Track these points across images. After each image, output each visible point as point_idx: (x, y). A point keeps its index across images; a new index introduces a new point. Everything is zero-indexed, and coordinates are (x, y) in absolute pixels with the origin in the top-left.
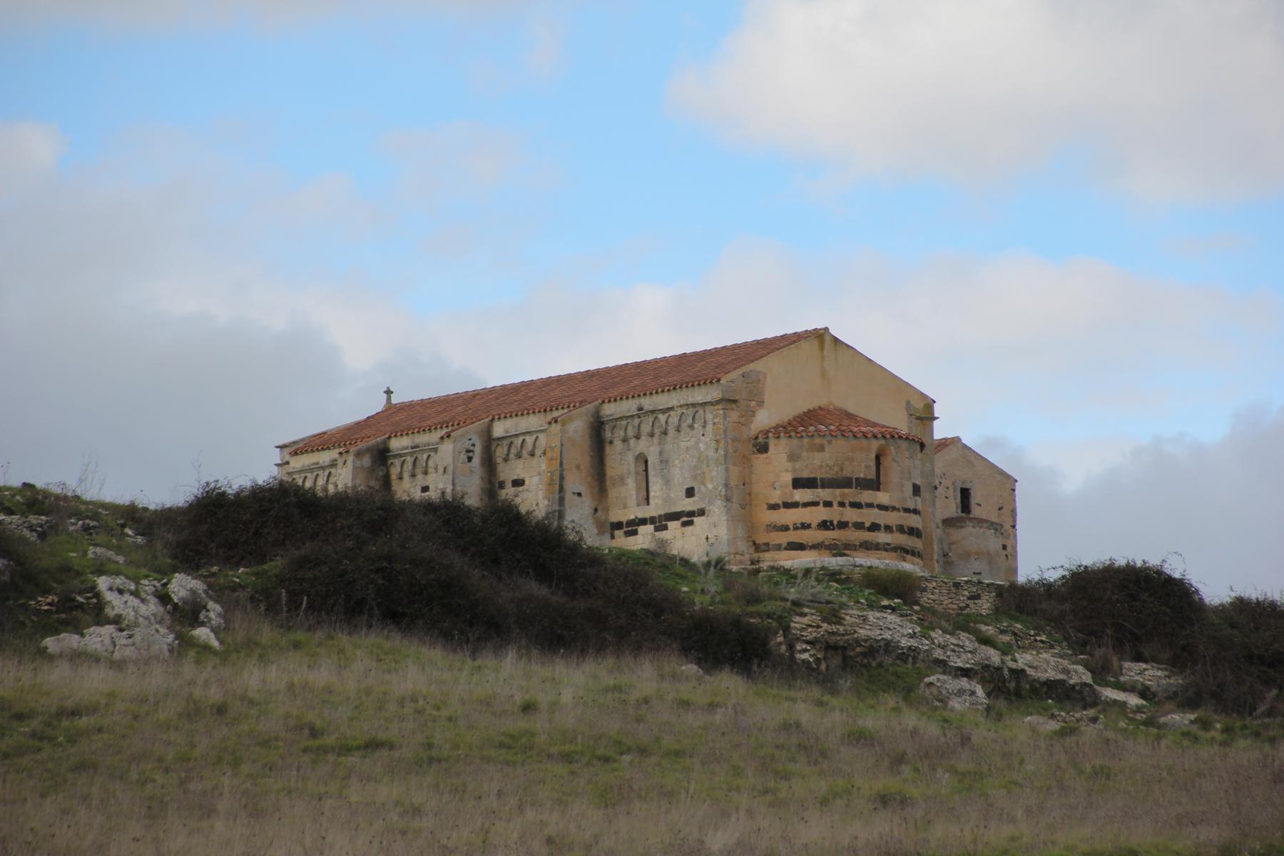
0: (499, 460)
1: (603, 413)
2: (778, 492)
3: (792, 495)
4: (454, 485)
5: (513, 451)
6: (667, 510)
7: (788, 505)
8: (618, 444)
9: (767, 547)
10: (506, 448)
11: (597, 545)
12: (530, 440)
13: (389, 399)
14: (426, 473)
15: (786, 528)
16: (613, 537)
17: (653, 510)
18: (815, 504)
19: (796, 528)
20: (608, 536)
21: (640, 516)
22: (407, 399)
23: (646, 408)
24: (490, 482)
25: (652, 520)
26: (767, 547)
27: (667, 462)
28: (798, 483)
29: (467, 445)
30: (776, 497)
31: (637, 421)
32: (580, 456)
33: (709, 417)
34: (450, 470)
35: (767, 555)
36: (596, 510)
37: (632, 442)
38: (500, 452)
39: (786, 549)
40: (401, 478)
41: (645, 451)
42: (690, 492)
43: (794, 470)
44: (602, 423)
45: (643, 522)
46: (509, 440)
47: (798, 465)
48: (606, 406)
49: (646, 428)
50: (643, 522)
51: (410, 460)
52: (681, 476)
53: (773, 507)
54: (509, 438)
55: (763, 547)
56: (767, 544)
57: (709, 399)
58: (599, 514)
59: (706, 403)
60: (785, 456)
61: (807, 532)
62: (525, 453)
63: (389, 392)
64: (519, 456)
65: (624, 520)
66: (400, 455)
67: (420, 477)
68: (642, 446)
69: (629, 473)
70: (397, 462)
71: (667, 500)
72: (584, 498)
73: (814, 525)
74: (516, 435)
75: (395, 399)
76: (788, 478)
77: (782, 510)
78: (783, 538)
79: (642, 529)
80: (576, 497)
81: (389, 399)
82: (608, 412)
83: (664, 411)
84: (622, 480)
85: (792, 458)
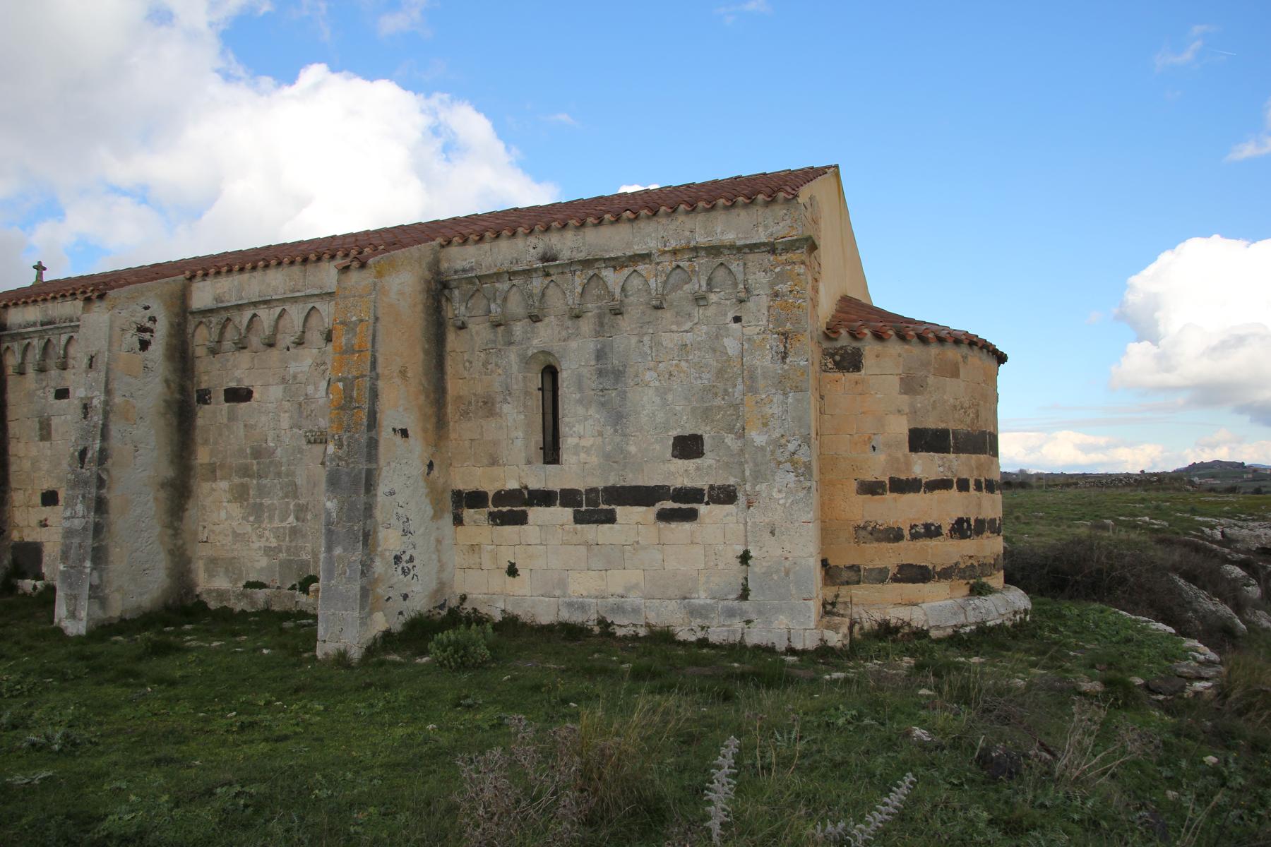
0: (200, 351)
1: (444, 265)
2: (882, 457)
3: (908, 465)
4: (108, 392)
5: (230, 334)
6: (613, 480)
7: (902, 486)
8: (480, 331)
9: (856, 575)
10: (215, 331)
11: (580, 620)
12: (266, 316)
13: (40, 276)
14: (64, 367)
15: (895, 535)
16: (458, 521)
17: (580, 467)
18: (944, 484)
19: (915, 536)
20: (448, 518)
21: (534, 484)
22: (62, 275)
23: (565, 255)
24: (183, 390)
25: (569, 498)
26: (856, 575)
27: (618, 375)
28: (922, 440)
29: (141, 317)
30: (877, 467)
31: (537, 283)
32: (402, 348)
33: (759, 279)
34: (101, 363)
35: (859, 592)
36: (431, 466)
37: (54, 373)
38: (202, 338)
39: (896, 580)
40: (21, 372)
41: (555, 347)
42: (688, 447)
43: (914, 411)
44: (445, 285)
45: (545, 498)
46: (225, 315)
47: (920, 401)
48: (454, 251)
49: (557, 302)
50: (545, 498)
51: (37, 343)
52: (658, 408)
53: (871, 488)
54: (221, 312)
55: (846, 575)
56: (854, 568)
57: (761, 237)
58: (435, 472)
59: (753, 247)
60: (896, 381)
61: (933, 543)
62: (255, 341)
63: (40, 268)
64: (241, 346)
65: (491, 489)
66: (22, 336)
67: (54, 373)
68: (545, 336)
69: (508, 391)
70: (17, 347)
71: (614, 457)
72: (411, 440)
73: (945, 530)
74: (239, 307)
75: (47, 277)
76: (900, 428)
77: (889, 496)
78: (891, 556)
79: (537, 514)
80: (398, 438)
81: (40, 276)
82: (459, 265)
83: (616, 263)
84: (488, 406)
85: (910, 385)
